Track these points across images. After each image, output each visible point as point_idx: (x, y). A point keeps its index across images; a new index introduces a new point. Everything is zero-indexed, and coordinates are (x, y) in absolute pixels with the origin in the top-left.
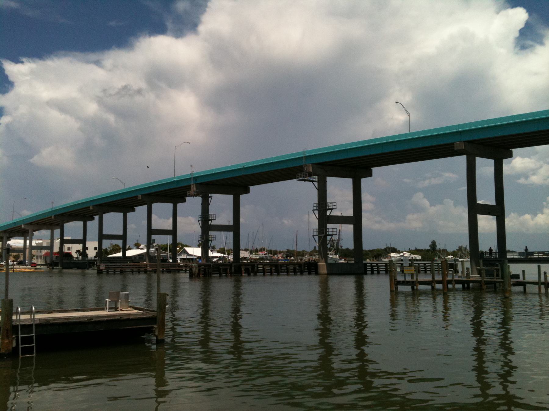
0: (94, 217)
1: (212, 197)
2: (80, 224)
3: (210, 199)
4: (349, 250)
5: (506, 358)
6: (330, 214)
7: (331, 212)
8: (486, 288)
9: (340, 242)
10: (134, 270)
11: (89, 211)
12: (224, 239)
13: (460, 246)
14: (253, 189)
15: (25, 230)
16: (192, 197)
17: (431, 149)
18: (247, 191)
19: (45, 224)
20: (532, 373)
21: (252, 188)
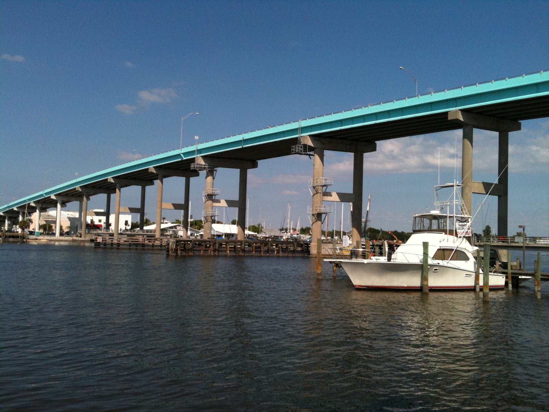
0: (376, 142)
1: (216, 170)
2: (138, 188)
3: (215, 172)
4: (398, 233)
5: (478, 387)
6: (326, 190)
7: (326, 189)
8: (66, 224)
9: (367, 224)
10: (110, 246)
11: (147, 174)
12: (309, 218)
13: (519, 232)
14: (260, 162)
15: (51, 200)
16: (299, 155)
17: (511, 110)
18: (255, 165)
19: (100, 188)
20: (250, 313)
21: (260, 162)
